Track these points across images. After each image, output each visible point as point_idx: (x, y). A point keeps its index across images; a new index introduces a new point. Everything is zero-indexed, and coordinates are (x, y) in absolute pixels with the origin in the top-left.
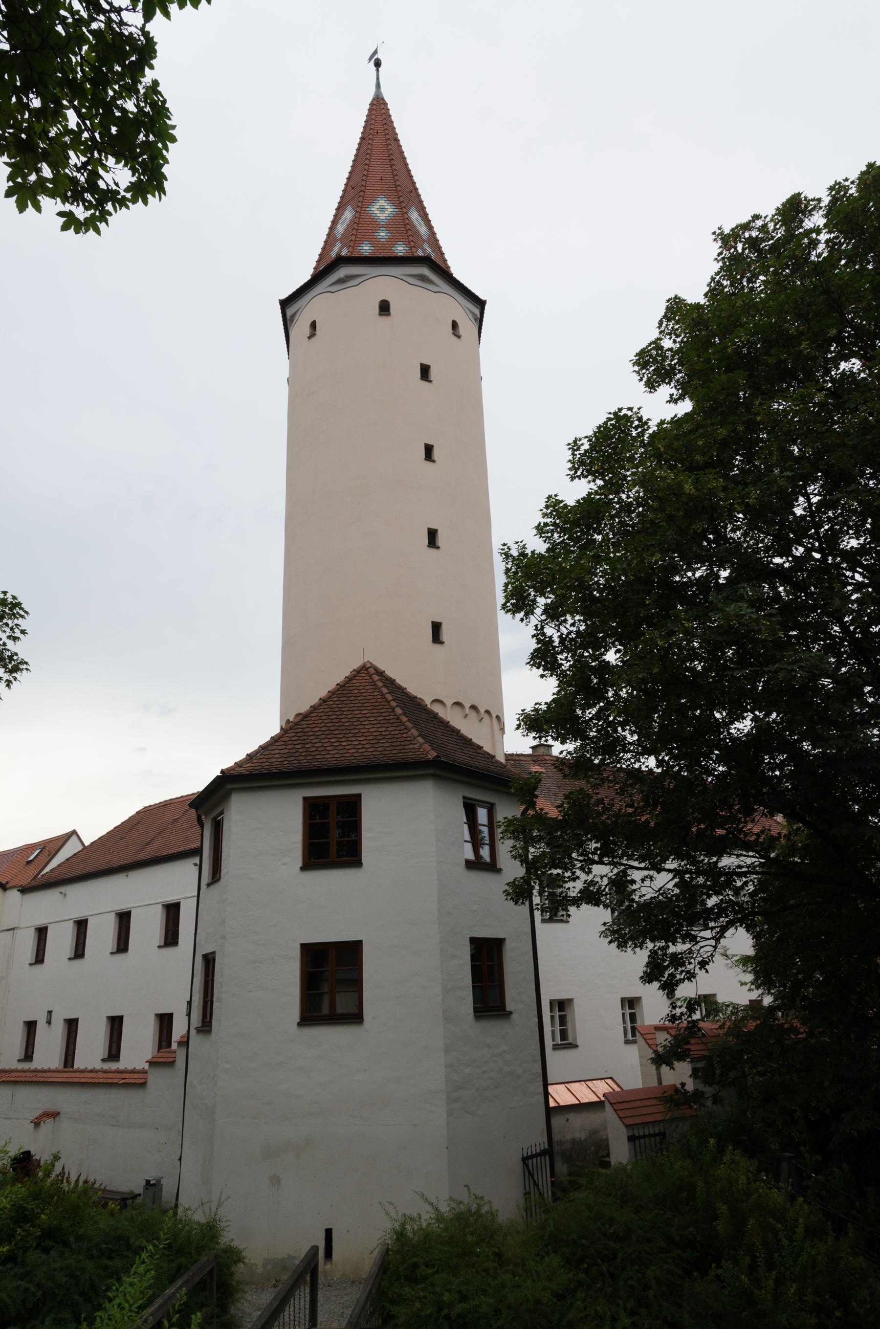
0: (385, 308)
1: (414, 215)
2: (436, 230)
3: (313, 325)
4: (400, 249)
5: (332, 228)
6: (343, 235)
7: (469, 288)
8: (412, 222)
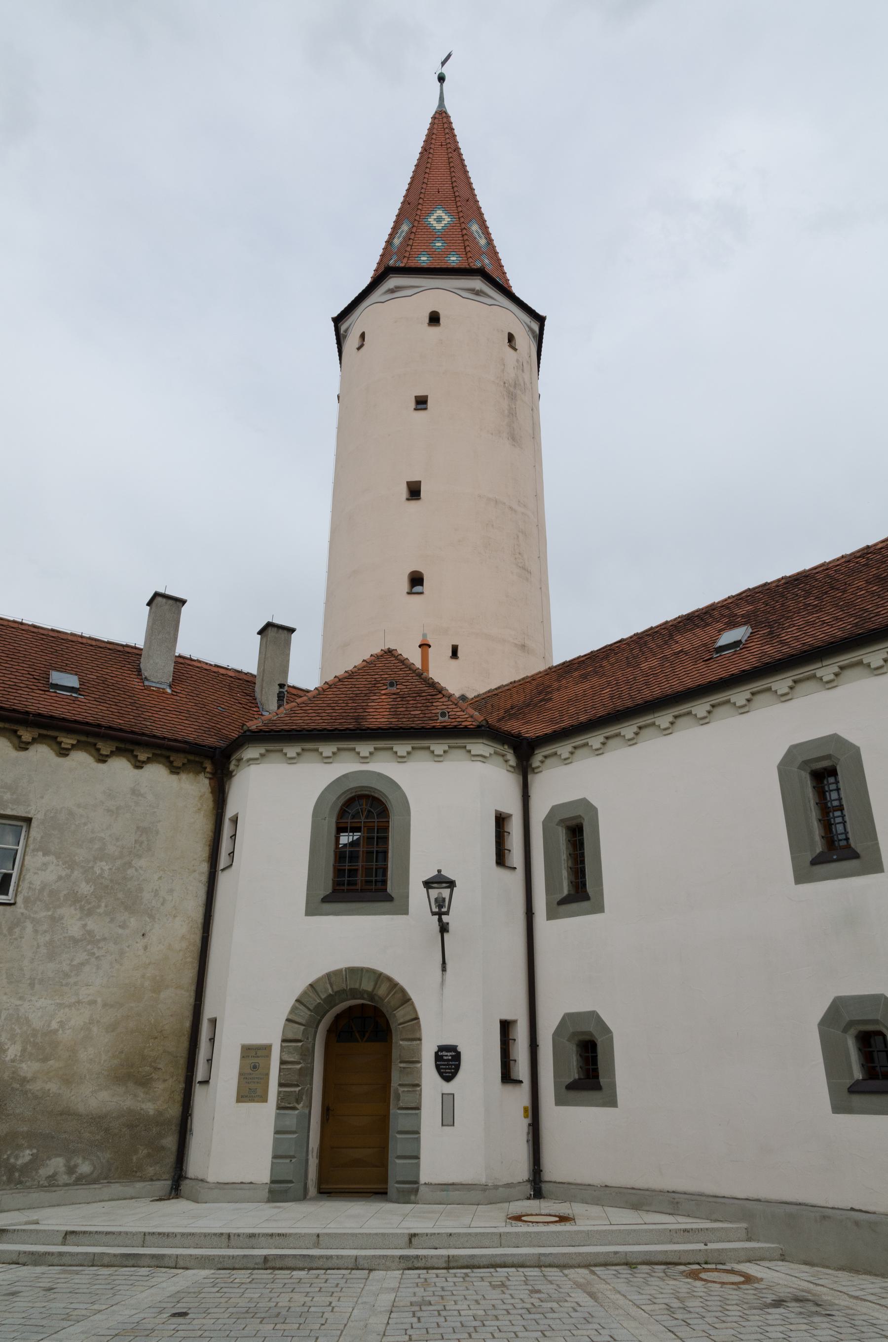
0: (434, 319)
1: (475, 228)
2: (493, 237)
3: (363, 336)
4: (454, 260)
5: (389, 242)
6: (399, 249)
7: (525, 301)
8: (472, 233)
